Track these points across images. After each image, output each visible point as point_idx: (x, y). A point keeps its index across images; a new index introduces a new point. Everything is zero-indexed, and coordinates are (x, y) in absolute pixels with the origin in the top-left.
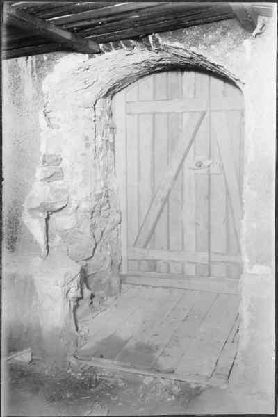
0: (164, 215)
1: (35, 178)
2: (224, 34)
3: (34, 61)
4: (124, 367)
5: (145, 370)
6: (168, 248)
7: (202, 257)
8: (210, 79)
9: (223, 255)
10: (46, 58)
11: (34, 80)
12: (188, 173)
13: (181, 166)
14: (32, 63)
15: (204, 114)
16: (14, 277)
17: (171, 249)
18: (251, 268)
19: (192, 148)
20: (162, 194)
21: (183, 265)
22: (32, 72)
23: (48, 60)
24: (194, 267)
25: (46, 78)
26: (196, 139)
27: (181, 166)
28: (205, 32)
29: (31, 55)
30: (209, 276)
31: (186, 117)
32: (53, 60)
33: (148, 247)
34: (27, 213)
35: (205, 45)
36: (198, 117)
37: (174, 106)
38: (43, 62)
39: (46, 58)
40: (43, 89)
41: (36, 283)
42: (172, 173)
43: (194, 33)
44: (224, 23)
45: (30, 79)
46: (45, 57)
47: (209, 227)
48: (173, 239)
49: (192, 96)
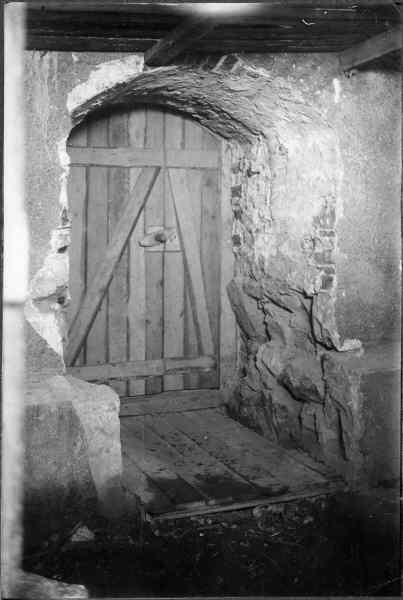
0: (102, 315)
1: (50, 247)
2: (314, 67)
3: (55, 61)
4: (223, 504)
5: (250, 500)
6: (107, 361)
7: (155, 367)
8: (184, 124)
9: (181, 359)
10: (75, 59)
11: (54, 91)
12: (137, 255)
13: (127, 242)
14: (51, 61)
15: (158, 169)
16: (38, 411)
17: (111, 361)
18: (342, 345)
19: (141, 217)
20: (98, 282)
21: (128, 383)
22: (50, 78)
23: (80, 62)
24: (142, 382)
25: (74, 91)
26: (147, 204)
27: (127, 242)
28: (295, 62)
29: (51, 50)
30: (163, 391)
31: (134, 174)
32: (89, 64)
33: (77, 363)
34: (32, 306)
35: (295, 78)
36: (151, 175)
37: (120, 156)
38: (70, 63)
39: (75, 59)
40: (68, 105)
41: (78, 413)
42: (115, 251)
43: (284, 61)
44: (316, 55)
45: (46, 89)
46: (75, 57)
47: (162, 322)
48: (113, 348)
49: (141, 146)
